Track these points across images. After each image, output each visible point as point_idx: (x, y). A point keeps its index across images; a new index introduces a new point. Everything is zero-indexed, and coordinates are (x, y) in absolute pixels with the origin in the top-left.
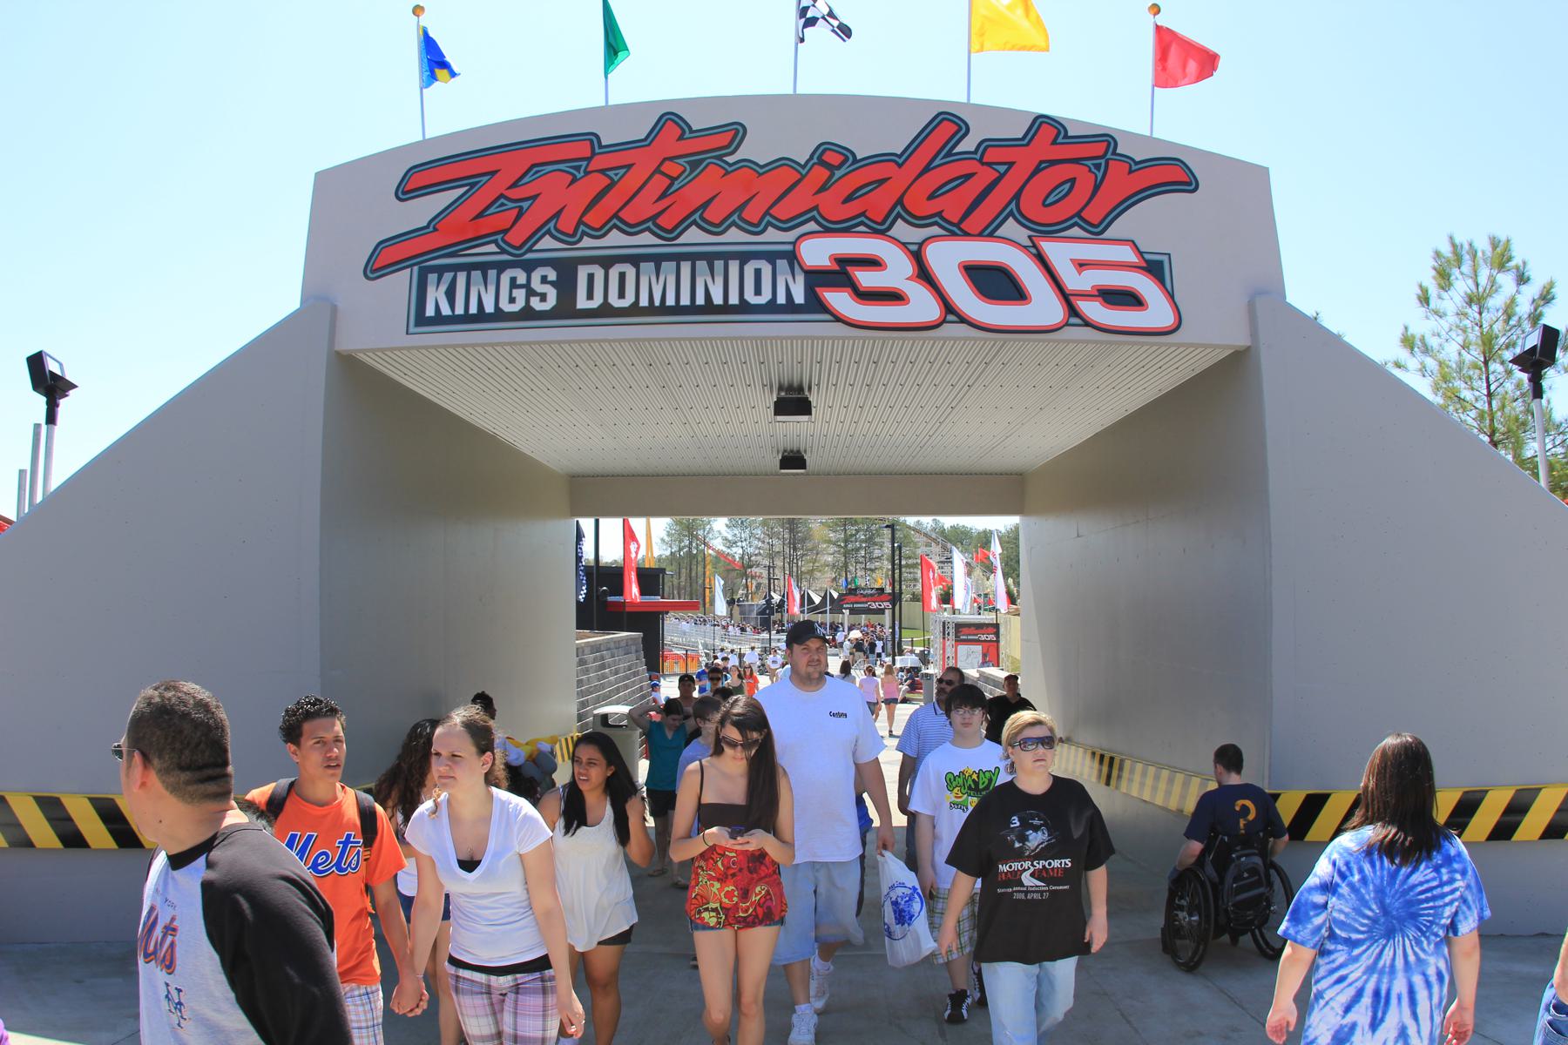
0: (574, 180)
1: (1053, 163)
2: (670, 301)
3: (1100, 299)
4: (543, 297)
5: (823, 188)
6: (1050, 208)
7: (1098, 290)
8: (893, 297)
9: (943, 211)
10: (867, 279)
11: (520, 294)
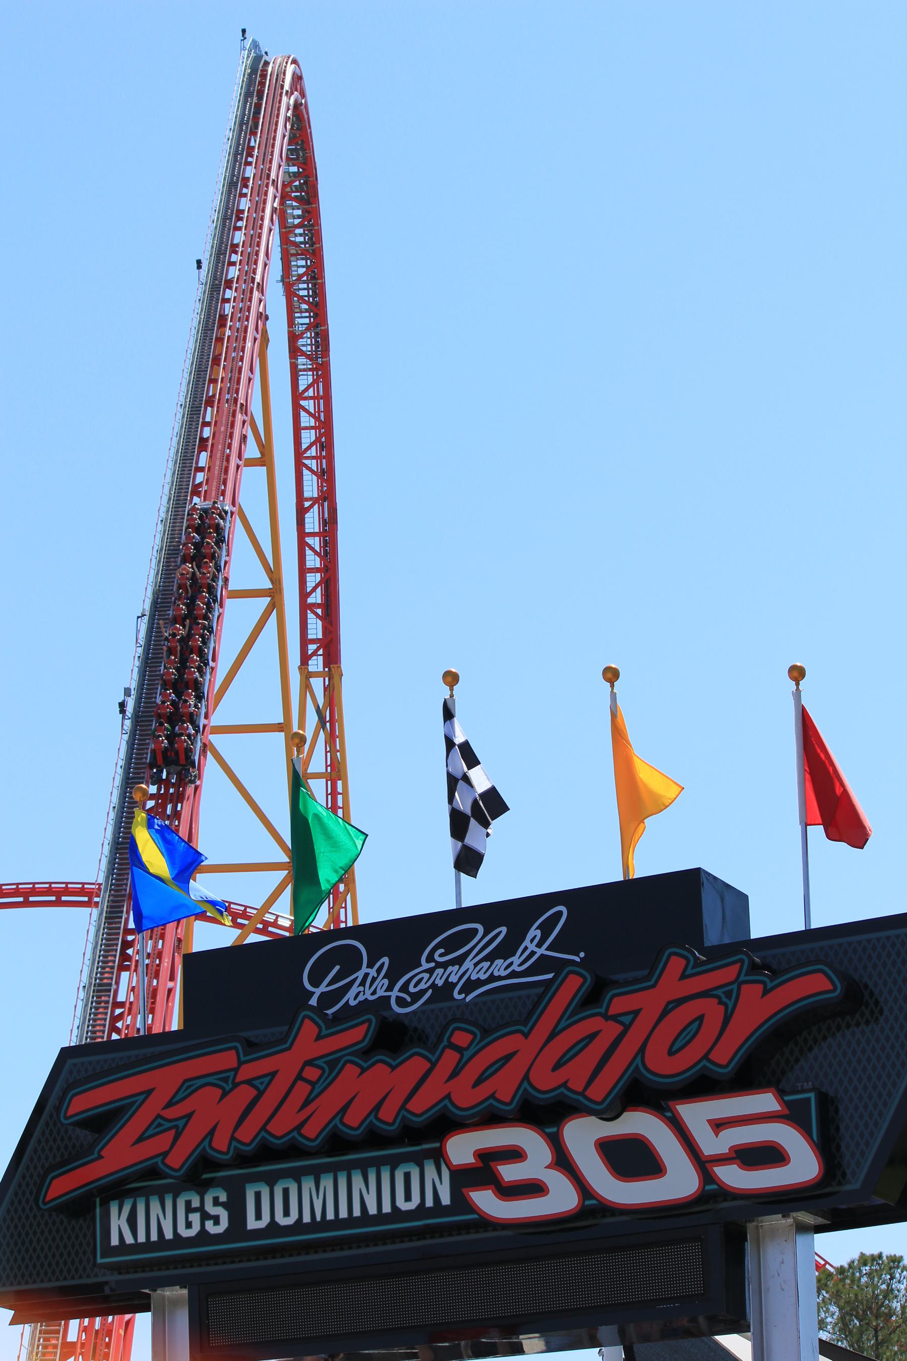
0: (225, 1094)
1: (680, 1002)
2: (330, 1216)
3: (738, 1161)
4: (216, 1220)
5: (454, 1074)
6: (678, 1055)
7: (736, 1152)
8: (535, 1189)
9: (568, 1081)
10: (509, 1172)
11: (195, 1218)
